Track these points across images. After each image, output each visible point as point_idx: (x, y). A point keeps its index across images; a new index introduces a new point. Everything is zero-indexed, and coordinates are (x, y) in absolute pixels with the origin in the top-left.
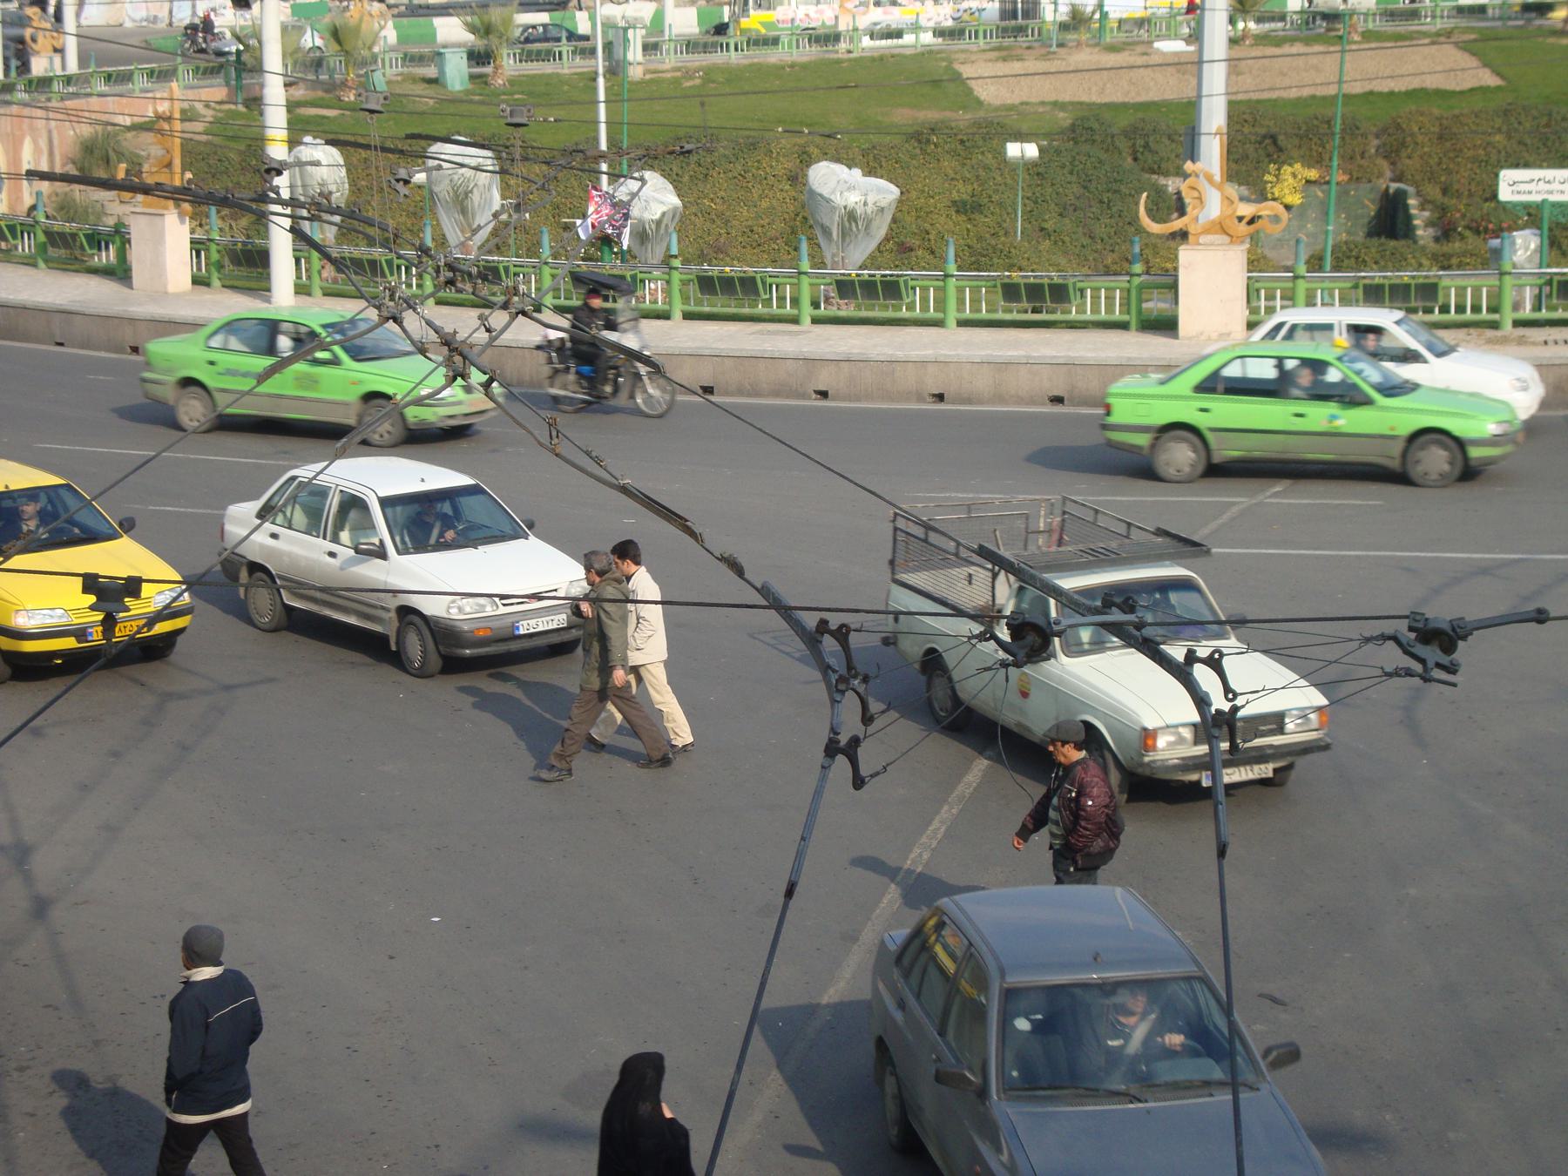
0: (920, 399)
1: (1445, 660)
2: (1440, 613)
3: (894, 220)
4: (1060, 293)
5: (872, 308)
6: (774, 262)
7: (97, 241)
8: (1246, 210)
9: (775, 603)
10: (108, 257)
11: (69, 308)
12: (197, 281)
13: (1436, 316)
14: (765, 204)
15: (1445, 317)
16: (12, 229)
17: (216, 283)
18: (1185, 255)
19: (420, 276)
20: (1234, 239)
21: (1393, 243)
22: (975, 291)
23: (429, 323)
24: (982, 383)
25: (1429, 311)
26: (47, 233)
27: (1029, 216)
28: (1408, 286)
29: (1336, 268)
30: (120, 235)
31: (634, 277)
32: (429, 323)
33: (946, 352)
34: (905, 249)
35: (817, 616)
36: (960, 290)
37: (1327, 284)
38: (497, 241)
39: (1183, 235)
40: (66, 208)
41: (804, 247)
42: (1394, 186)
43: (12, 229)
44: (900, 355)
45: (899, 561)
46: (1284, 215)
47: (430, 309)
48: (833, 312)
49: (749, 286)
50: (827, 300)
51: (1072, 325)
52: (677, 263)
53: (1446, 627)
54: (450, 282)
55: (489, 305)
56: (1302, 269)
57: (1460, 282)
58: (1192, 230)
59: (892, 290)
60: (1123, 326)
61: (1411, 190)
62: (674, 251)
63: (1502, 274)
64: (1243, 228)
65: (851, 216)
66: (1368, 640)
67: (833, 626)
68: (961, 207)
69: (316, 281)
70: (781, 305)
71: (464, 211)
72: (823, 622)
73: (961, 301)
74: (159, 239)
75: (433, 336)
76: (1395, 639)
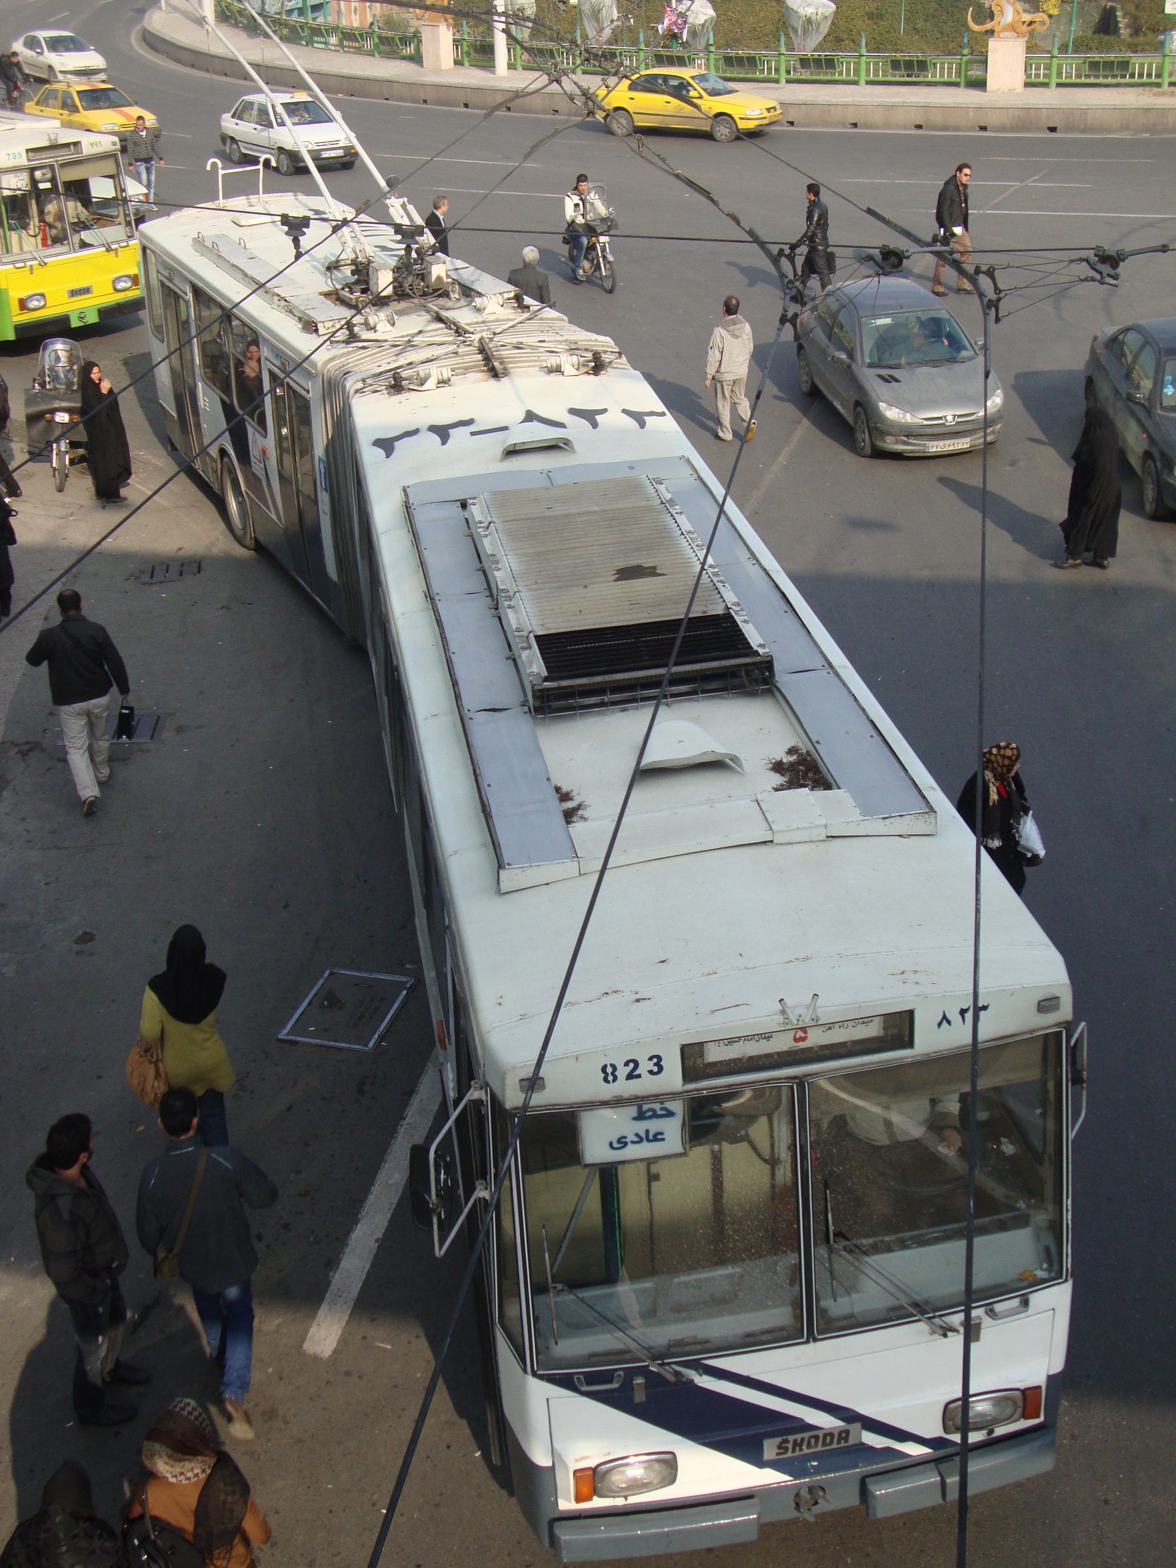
0: (844, 126)
1: (1112, 272)
2: (1111, 249)
3: (833, 23)
4: (922, 66)
5: (819, 74)
6: (766, 48)
7: (405, 41)
8: (1027, 17)
9: (756, 239)
10: (410, 50)
11: (394, 79)
12: (457, 63)
13: (1128, 80)
14: (762, 14)
15: (1132, 80)
16: (361, 35)
17: (466, 63)
18: (992, 44)
19: (574, 58)
20: (1019, 34)
21: (1107, 38)
22: (876, 64)
23: (575, 83)
24: (878, 117)
25: (1124, 77)
26: (379, 37)
27: (906, 23)
28: (1113, 62)
29: (1075, 51)
30: (417, 37)
31: (689, 57)
32: (575, 83)
33: (859, 99)
34: (839, 40)
35: (778, 247)
36: (868, 64)
37: (1069, 61)
38: (614, 39)
39: (991, 33)
40: (389, 23)
41: (783, 39)
42: (1110, 4)
43: (361, 35)
44: (834, 101)
45: (946, 214)
46: (1048, 21)
47: (579, 77)
48: (798, 76)
49: (752, 61)
50: (795, 69)
51: (929, 84)
52: (712, 49)
53: (1113, 254)
54: (587, 60)
55: (608, 73)
56: (1056, 52)
57: (1141, 60)
58: (996, 29)
59: (830, 63)
60: (956, 84)
61: (1118, 6)
62: (711, 42)
63: (1164, 56)
64: (1025, 28)
65: (809, 21)
66: (1072, 261)
67: (984, 268)
68: (871, 16)
69: (519, 63)
70: (769, 72)
71: (597, 20)
72: (781, 251)
73: (868, 70)
74: (436, 40)
75: (578, 91)
76: (1087, 260)
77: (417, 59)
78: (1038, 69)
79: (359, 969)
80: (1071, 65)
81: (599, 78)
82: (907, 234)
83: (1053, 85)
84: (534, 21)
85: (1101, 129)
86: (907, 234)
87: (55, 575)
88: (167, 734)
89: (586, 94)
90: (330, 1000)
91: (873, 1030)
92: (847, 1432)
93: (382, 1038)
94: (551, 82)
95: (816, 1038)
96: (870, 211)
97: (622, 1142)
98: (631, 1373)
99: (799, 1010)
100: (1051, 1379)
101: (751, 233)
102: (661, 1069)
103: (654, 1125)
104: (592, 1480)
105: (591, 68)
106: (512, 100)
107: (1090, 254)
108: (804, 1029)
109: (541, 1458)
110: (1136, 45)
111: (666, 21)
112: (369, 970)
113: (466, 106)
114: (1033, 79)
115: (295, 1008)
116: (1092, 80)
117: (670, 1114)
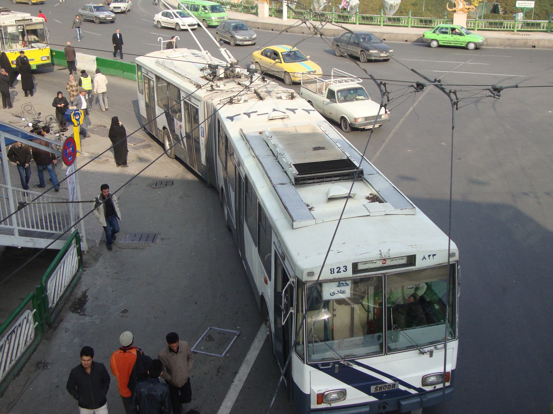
0: (403, 41)
1: (498, 94)
2: (498, 86)
4: (430, 22)
6: (376, 14)
7: (253, 8)
8: (467, 7)
9: (372, 78)
10: (254, 11)
13: (502, 29)
18: (455, 15)
22: (414, 21)
26: (244, 7)
27: (426, 6)
30: (256, 7)
36: (412, 20)
38: (324, 9)
39: (455, 11)
41: (382, 11)
48: (387, 24)
49: (371, 18)
55: (322, 21)
56: (477, 19)
59: (398, 20)
64: (466, 10)
65: (392, 5)
67: (453, 91)
68: (413, 4)
71: (319, 3)
73: (411, 23)
77: (256, 14)
78: (471, 24)
79: (220, 327)
80: (482, 23)
81: (319, 23)
82: (426, 78)
83: (476, 30)
84: (297, 3)
85: (492, 46)
86: (426, 78)
87: (123, 184)
88: (158, 241)
89: (314, 27)
90: (209, 338)
91: (404, 261)
92: (395, 384)
93: (227, 353)
94: (303, 23)
95: (389, 263)
96: (412, 70)
97: (334, 294)
98: (335, 363)
99: (385, 254)
100: (452, 371)
101: (371, 76)
102: (346, 270)
103: (343, 288)
104: (321, 398)
105: (316, 19)
106: (289, 28)
107: (490, 87)
108: (385, 260)
109: (307, 392)
110: (505, 17)
111: (342, 5)
112: (224, 328)
113: (272, 30)
114: (469, 27)
115: (197, 340)
116: (490, 29)
117: (347, 285)
